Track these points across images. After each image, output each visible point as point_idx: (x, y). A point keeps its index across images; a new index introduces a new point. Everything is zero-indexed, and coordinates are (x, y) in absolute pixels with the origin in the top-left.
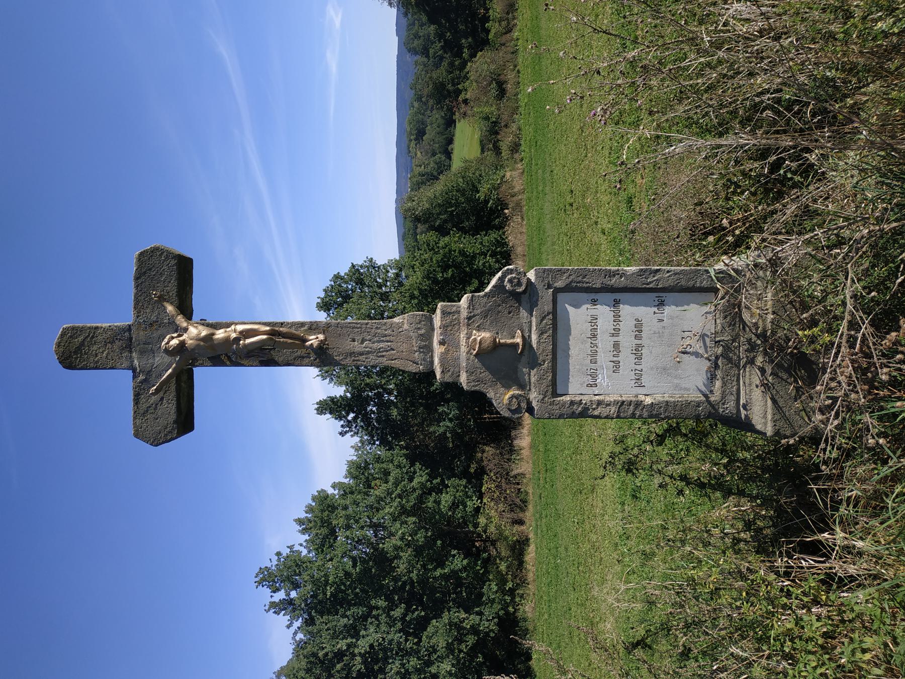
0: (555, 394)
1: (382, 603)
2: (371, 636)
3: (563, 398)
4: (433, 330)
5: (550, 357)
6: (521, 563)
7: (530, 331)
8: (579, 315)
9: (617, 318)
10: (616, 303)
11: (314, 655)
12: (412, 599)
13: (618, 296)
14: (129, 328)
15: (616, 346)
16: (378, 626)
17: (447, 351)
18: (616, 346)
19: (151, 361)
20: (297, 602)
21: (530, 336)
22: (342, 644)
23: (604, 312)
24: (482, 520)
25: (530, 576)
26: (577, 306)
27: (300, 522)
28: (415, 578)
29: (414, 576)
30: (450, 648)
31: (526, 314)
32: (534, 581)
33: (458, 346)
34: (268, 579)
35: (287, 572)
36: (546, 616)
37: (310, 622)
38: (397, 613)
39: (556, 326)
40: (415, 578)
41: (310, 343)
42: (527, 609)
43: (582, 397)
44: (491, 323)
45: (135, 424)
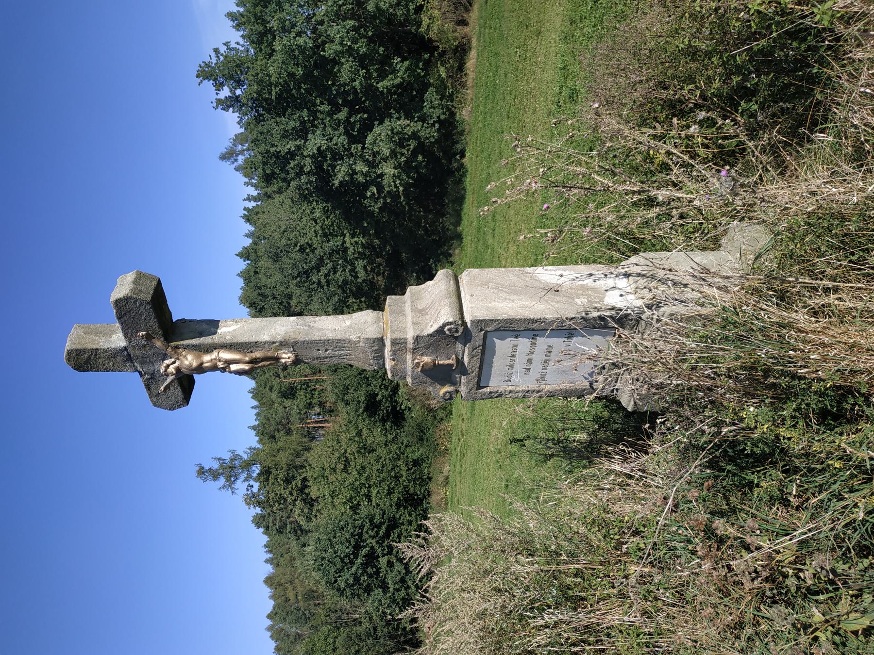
0: (479, 387)
1: (326, 108)
2: (316, 142)
3: (485, 389)
4: (384, 345)
5: (477, 370)
6: (461, 68)
7: (463, 355)
8: (502, 346)
9: (533, 345)
10: (535, 336)
11: (268, 152)
12: (353, 106)
13: (536, 333)
14: (125, 349)
15: (530, 361)
16: (324, 129)
17: (396, 365)
18: (530, 361)
19: (152, 368)
20: (244, 101)
21: (463, 358)
22: (291, 145)
23: (524, 343)
24: (425, 21)
25: (470, 83)
26: (502, 339)
27: (231, 16)
28: (358, 87)
29: (357, 84)
30: (393, 153)
31: (461, 346)
32: (473, 87)
33: (405, 362)
34: (206, 73)
35: (225, 71)
36: (481, 125)
37: (259, 119)
38: (342, 115)
39: (485, 353)
40: (358, 87)
41: (283, 361)
42: (464, 114)
43: (498, 388)
44: (432, 351)
45: (152, 401)
